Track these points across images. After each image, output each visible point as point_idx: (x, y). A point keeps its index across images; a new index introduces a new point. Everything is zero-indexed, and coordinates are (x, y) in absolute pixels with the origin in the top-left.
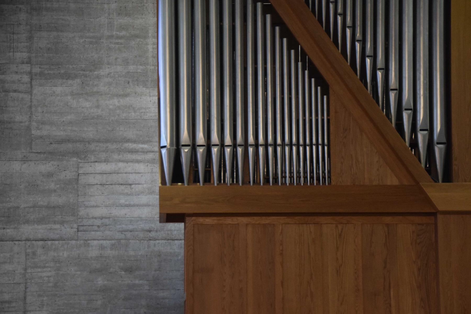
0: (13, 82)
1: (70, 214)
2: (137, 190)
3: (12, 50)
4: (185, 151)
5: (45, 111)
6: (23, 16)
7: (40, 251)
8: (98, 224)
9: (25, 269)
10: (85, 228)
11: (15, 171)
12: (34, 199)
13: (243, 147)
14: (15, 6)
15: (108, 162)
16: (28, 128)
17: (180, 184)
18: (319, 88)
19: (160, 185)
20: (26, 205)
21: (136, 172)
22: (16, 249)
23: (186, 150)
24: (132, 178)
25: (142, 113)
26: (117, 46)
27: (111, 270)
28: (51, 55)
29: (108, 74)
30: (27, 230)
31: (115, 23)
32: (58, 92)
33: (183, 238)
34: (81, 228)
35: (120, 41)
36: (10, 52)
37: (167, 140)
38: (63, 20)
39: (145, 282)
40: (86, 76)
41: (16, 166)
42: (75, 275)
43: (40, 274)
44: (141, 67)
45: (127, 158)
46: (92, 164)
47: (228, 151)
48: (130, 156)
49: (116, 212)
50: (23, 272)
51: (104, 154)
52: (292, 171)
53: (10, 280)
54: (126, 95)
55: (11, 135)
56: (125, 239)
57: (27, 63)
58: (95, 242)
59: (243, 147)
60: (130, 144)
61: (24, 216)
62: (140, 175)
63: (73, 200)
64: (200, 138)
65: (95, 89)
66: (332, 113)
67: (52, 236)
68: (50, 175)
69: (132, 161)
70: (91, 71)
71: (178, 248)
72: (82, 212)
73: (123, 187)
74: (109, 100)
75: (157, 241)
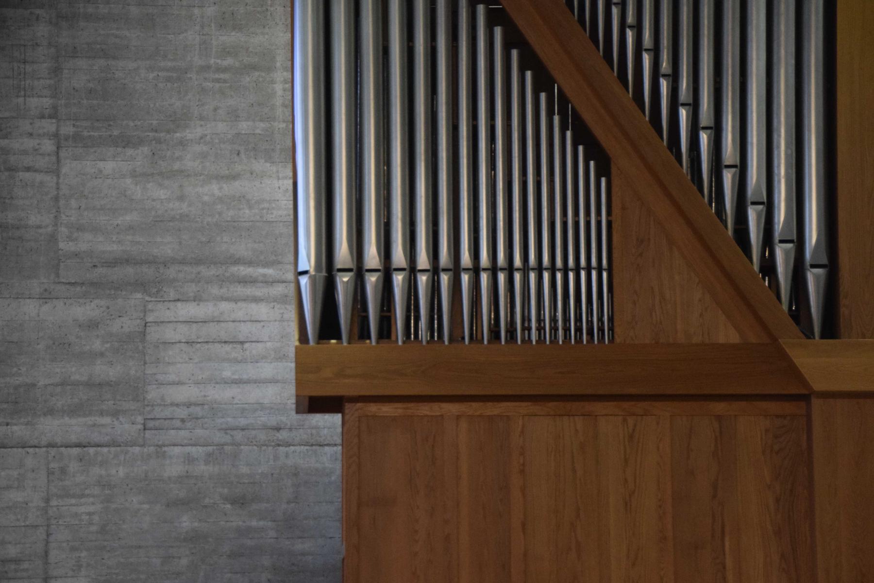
0: (25, 152)
1: (130, 397)
2: (254, 352)
3: (22, 93)
4: (343, 280)
5: (83, 207)
6: (42, 30)
7: (73, 466)
8: (182, 417)
9: (47, 500)
10: (157, 423)
11: (27, 318)
12: (63, 370)
13: (451, 273)
14: (29, 11)
15: (200, 300)
16: (53, 238)
17: (333, 341)
18: (592, 163)
19: (297, 343)
20: (48, 381)
21: (253, 319)
22: (29, 462)
23: (345, 279)
24: (245, 330)
25: (263, 209)
26: (217, 85)
27: (207, 501)
28: (95, 102)
29: (201, 138)
30: (50, 427)
31: (214, 43)
32: (108, 172)
33: (339, 441)
34: (151, 424)
35: (222, 76)
36: (18, 96)
37: (309, 261)
38: (116, 37)
39: (270, 523)
40: (159, 141)
41: (30, 308)
42: (139, 510)
43: (74, 509)
44: (262, 125)
45: (235, 294)
46: (171, 305)
47: (423, 280)
48: (240, 290)
49: (215, 393)
50: (43, 505)
51: (193, 285)
52: (542, 317)
53: (18, 520)
54: (234, 177)
55: (20, 250)
56: (232, 444)
57: (50, 117)
58: (177, 450)
59: (451, 273)
60: (242, 268)
61: (45, 401)
62: (259, 325)
63: (136, 371)
64: (372, 256)
65: (177, 166)
66: (616, 210)
67: (96, 437)
68: (92, 325)
69: (246, 299)
70: (168, 132)
71: (330, 460)
72: (153, 394)
73: (228, 348)
74: (202, 186)
75: (292, 448)
